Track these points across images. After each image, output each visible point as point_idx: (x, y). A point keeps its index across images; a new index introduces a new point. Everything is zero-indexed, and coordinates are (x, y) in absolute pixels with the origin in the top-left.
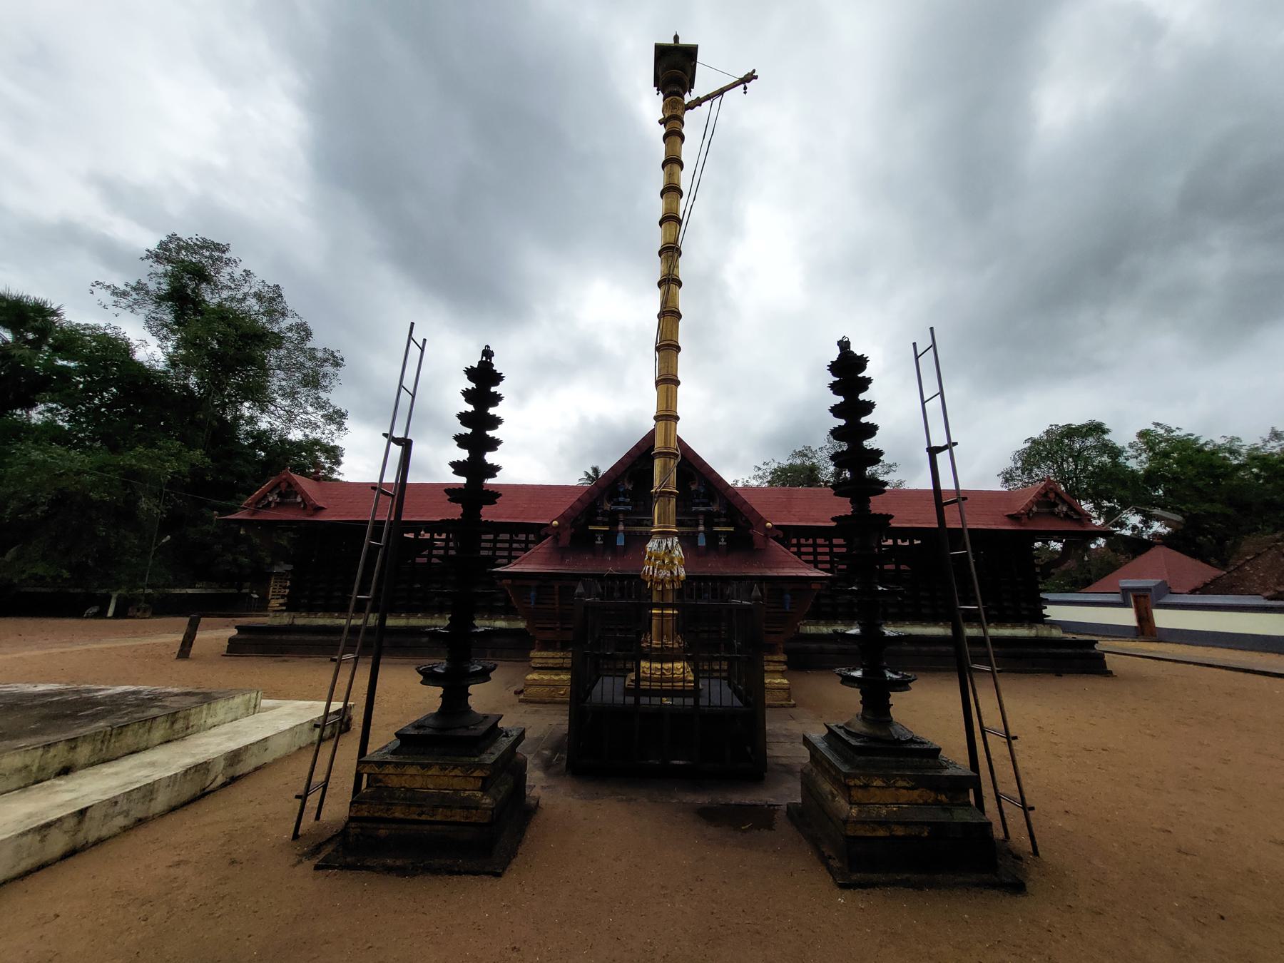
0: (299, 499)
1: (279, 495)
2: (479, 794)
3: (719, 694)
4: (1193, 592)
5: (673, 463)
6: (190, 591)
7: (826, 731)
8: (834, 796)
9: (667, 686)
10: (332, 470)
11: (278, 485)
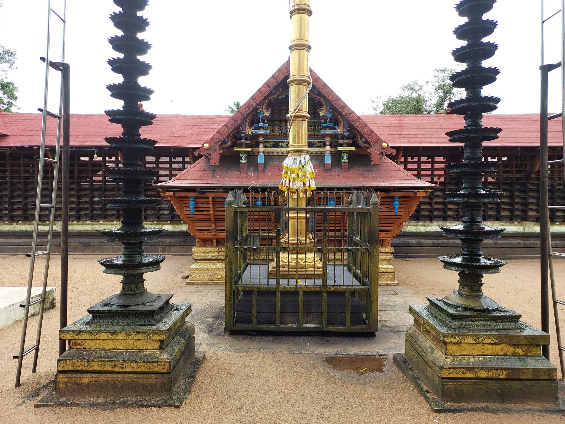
2: (158, 352)
3: (341, 277)
5: (305, 90)
7: (429, 303)
8: (433, 350)
9: (301, 271)
10: (10, 104)
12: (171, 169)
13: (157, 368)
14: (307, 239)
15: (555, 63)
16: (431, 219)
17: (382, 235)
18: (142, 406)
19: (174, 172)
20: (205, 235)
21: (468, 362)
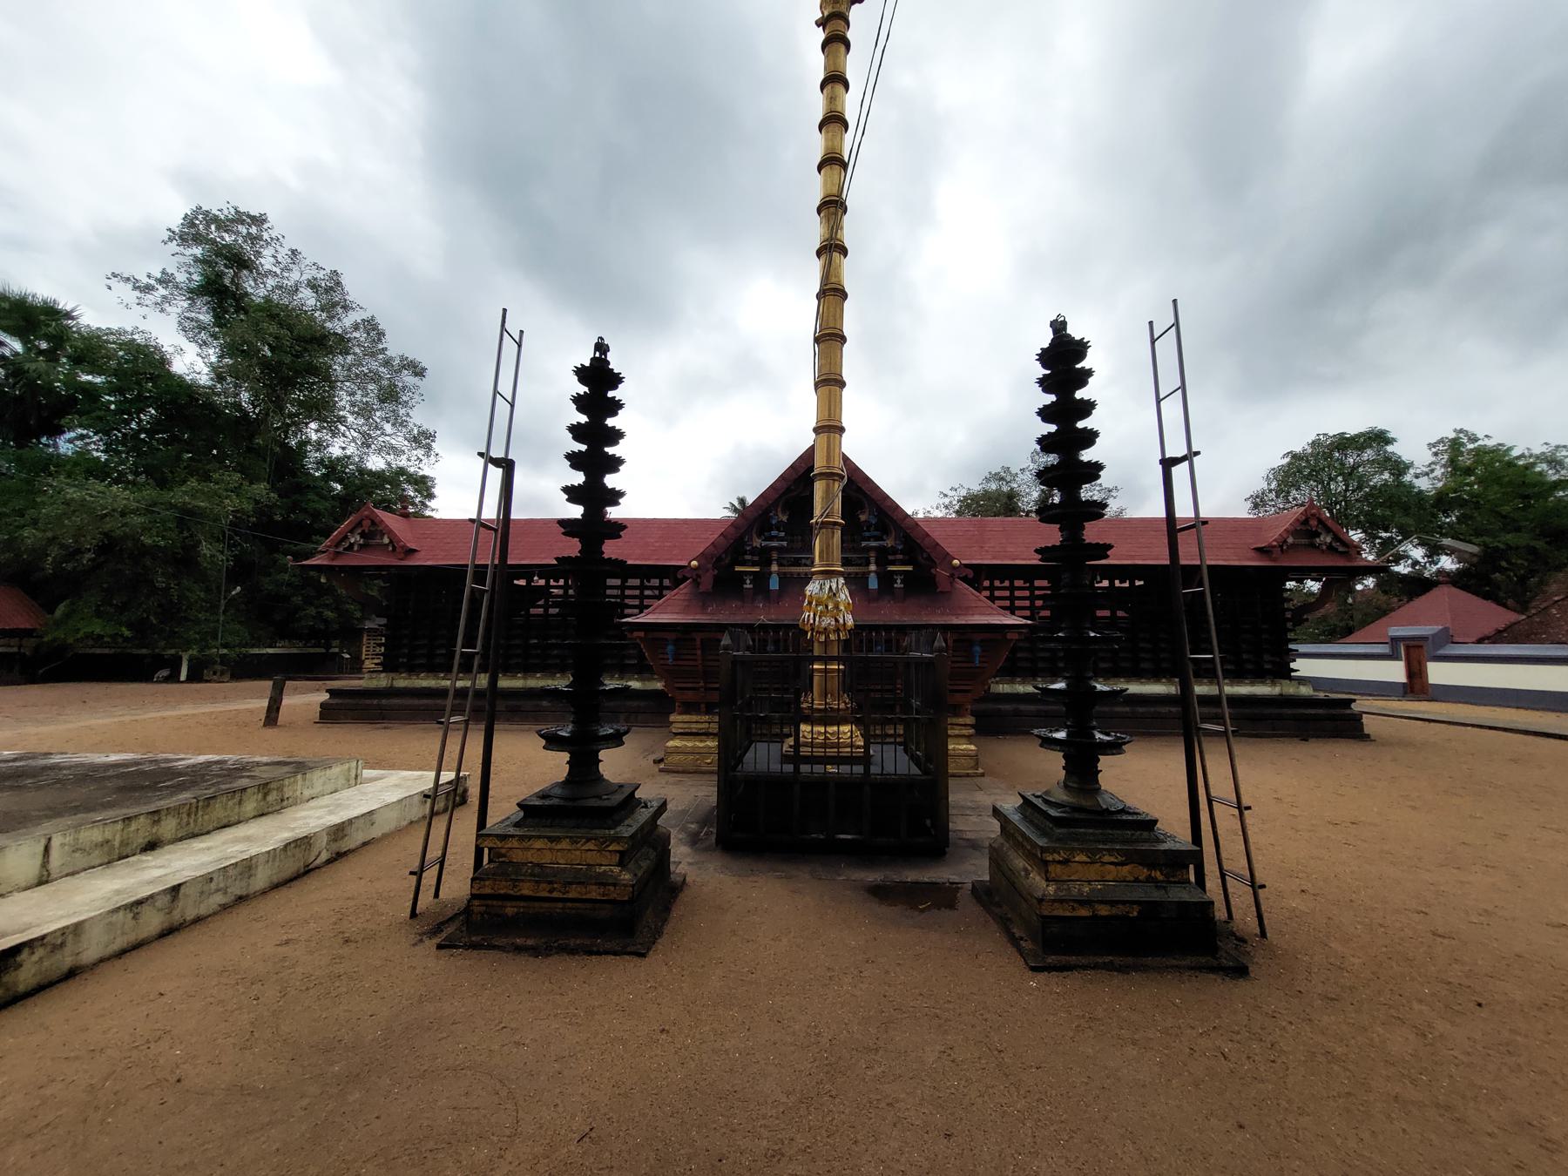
0: (386, 540)
1: (362, 535)
2: (616, 870)
3: (893, 761)
4: (1480, 641)
5: (838, 487)
6: (270, 651)
8: (1027, 873)
9: (832, 752)
11: (359, 524)
12: (642, 597)
13: (614, 894)
14: (842, 704)
15: (1179, 455)
16: (1030, 674)
17: (959, 698)
18: (590, 953)
19: (646, 602)
20: (690, 696)
21: (1080, 893)
